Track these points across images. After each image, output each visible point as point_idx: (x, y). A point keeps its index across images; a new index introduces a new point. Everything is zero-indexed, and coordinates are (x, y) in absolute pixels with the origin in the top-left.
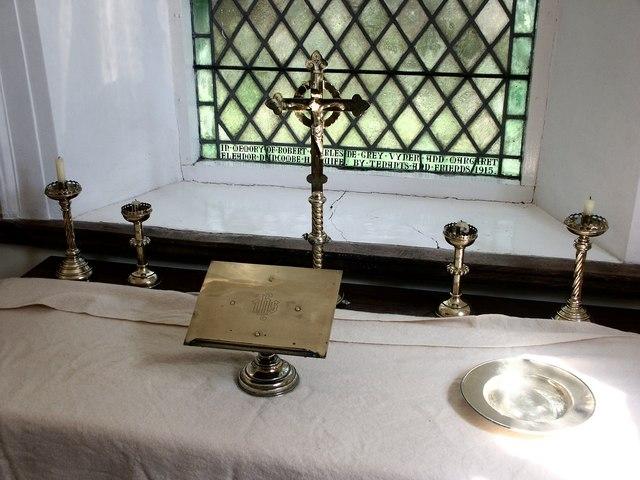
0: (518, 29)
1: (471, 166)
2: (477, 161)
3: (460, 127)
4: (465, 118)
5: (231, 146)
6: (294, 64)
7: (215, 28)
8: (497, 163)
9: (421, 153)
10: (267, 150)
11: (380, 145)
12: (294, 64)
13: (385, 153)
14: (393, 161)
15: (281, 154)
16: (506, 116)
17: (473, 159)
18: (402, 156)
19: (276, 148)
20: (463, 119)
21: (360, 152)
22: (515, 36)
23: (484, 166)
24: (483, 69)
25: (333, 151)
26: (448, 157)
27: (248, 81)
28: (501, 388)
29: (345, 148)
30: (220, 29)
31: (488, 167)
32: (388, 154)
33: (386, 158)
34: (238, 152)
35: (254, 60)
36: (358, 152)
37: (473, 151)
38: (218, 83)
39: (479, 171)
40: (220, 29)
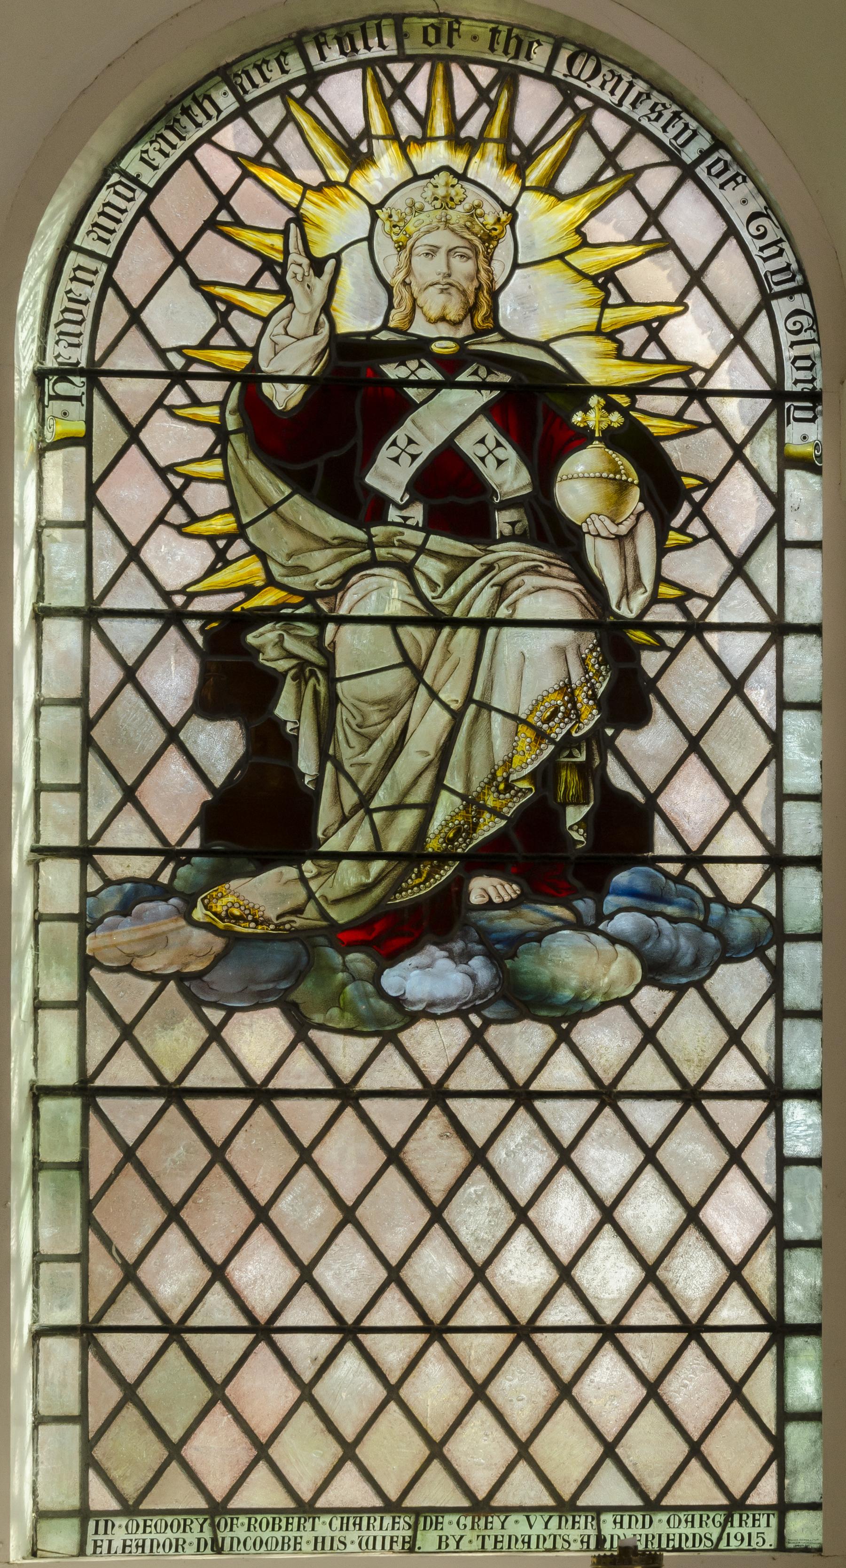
0: (793, 1229)
1: (715, 1533)
2: (729, 1519)
3: (744, 1039)
4: (654, 202)
5: (120, 1521)
6: (290, 1318)
7: (93, 1238)
8: (774, 1521)
9: (598, 1511)
10: (215, 1527)
11: (499, 1501)
12: (290, 1318)
13: (513, 1517)
14: (534, 1532)
15: (253, 1535)
16: (785, 1416)
17: (720, 1518)
18: (555, 1521)
19: (244, 1519)
20: (734, 241)
21: (454, 1518)
22: (784, 1246)
23: (745, 1531)
24: (724, 1315)
25: (388, 1520)
26: (664, 1516)
27: (608, 1358)
28: (526, 581)
29: (418, 1512)
30: (107, 1242)
31: (754, 1531)
32: (521, 1517)
33: (517, 1526)
34: (140, 1535)
35: (277, 1313)
36: (448, 1518)
37: (723, 1501)
38: (93, 1363)
39: (734, 1544)
40: (107, 1242)
